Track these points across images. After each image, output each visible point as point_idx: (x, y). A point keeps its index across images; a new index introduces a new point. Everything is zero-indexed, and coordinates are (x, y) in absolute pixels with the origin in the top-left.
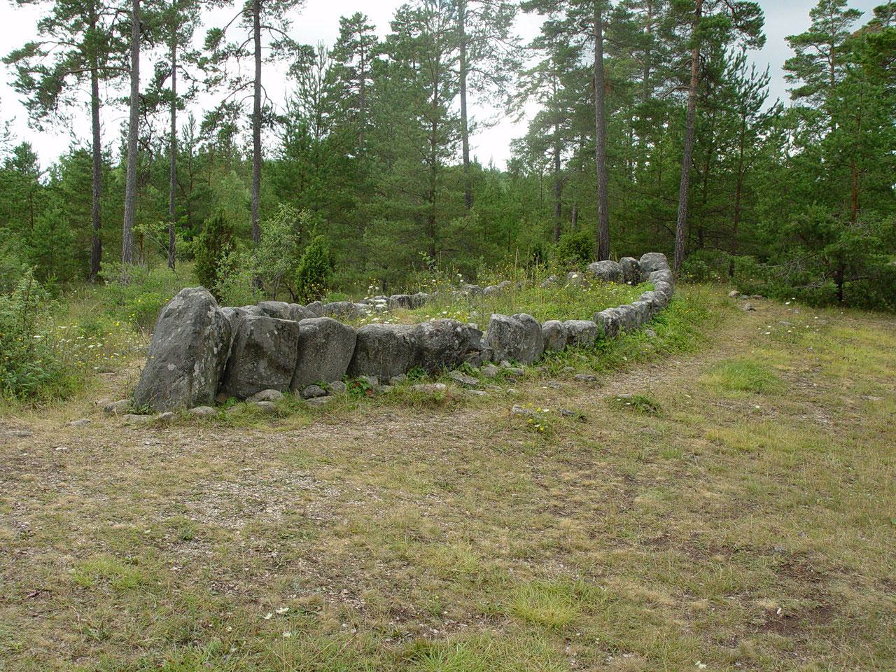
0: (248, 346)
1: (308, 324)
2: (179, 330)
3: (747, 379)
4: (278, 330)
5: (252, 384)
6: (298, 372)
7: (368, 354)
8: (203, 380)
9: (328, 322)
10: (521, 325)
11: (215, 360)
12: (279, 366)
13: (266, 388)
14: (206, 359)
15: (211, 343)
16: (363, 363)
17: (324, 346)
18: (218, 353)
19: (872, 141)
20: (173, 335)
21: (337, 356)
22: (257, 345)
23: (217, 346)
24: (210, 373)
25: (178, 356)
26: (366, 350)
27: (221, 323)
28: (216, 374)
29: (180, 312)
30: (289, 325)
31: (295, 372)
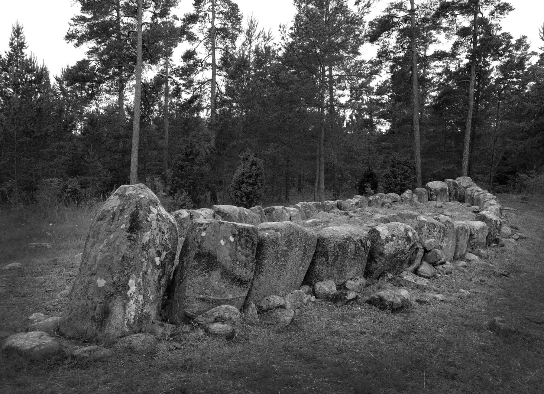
0: (199, 256)
1: (268, 229)
2: (112, 236)
3: (452, 231)
4: (234, 236)
5: (203, 300)
6: (256, 284)
7: (327, 259)
8: (141, 297)
9: (291, 227)
10: (443, 225)
11: (157, 273)
12: (235, 278)
13: (218, 303)
14: (146, 273)
15: (152, 251)
16: (321, 268)
17: (285, 254)
18: (161, 262)
19: (193, 159)
20: (105, 242)
21: (297, 263)
22: (209, 255)
23: (159, 254)
24: (151, 288)
25: (110, 269)
26: (325, 255)
27: (164, 228)
28: (158, 289)
29: (114, 215)
30: (247, 230)
31: (252, 283)
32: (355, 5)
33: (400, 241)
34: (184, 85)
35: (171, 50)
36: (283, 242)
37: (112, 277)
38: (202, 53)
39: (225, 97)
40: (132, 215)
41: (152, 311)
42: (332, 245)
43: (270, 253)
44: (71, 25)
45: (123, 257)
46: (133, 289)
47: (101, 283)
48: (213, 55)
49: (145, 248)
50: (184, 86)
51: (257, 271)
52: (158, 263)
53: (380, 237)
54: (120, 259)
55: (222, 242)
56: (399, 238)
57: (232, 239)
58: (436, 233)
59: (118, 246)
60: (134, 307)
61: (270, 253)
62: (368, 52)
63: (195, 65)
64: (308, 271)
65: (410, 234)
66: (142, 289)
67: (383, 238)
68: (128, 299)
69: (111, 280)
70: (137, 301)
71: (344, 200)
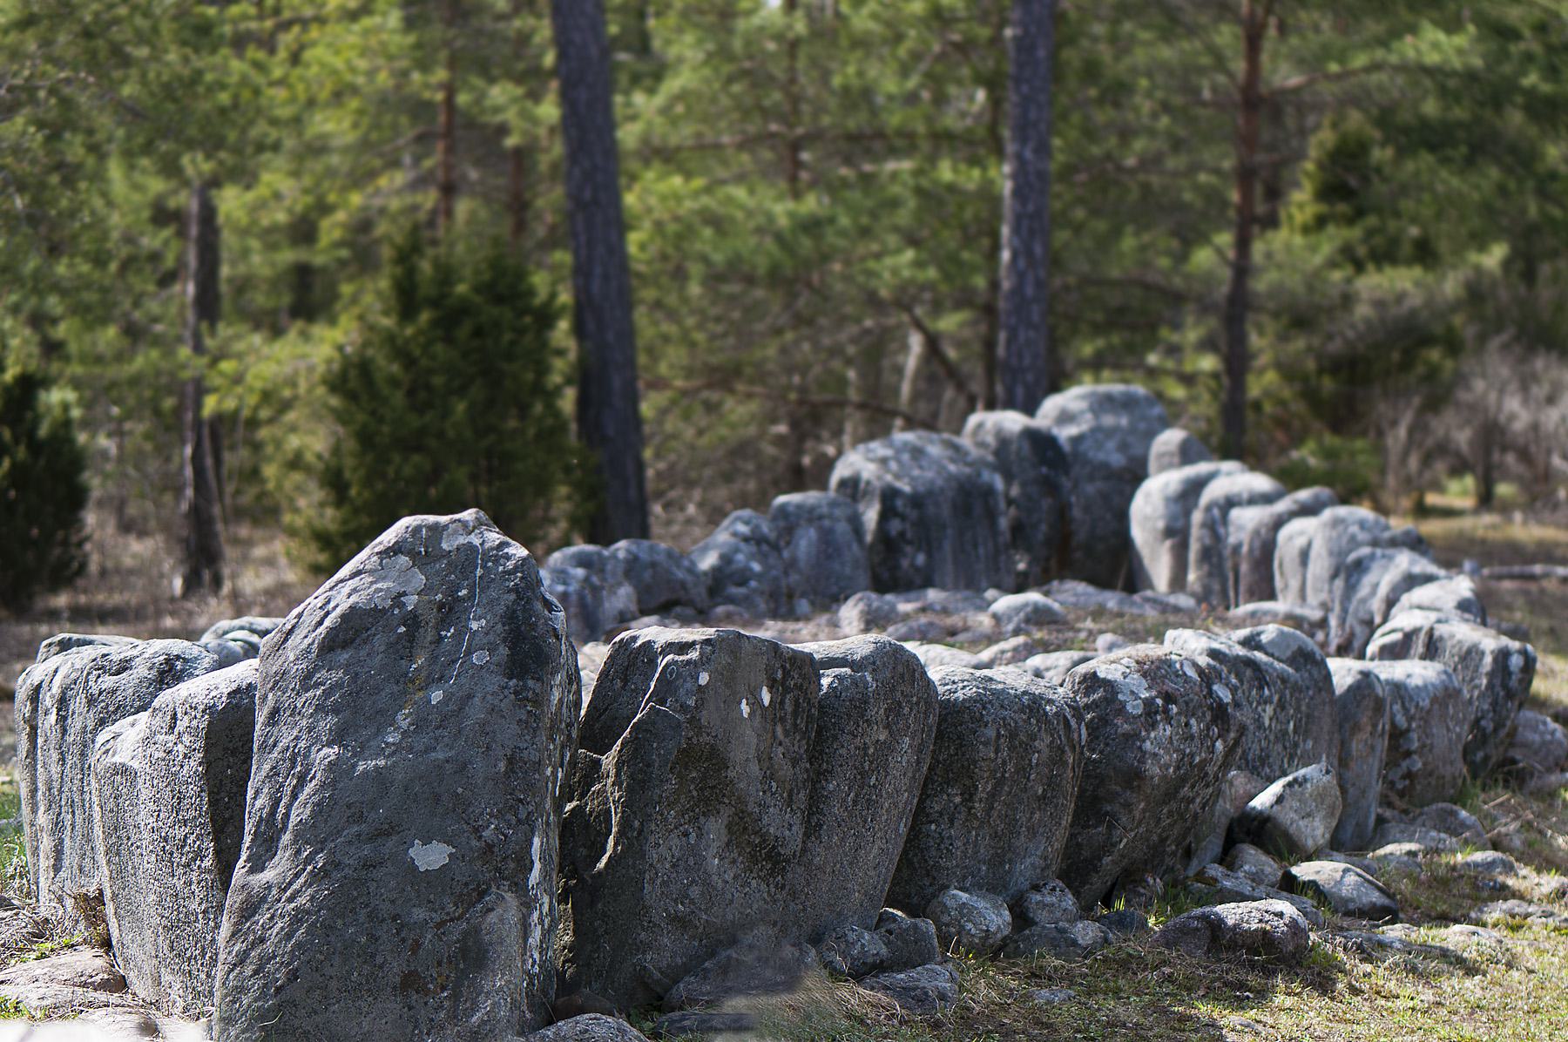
7: (969, 795)
33: (1193, 721)
36: (877, 711)
37: (477, 830)
39: (916, 342)
40: (510, 617)
42: (991, 732)
43: (843, 751)
44: (1439, 621)
45: (511, 761)
47: (431, 856)
51: (812, 829)
53: (1123, 704)
54: (502, 766)
56: (1189, 711)
58: (1269, 709)
59: (483, 724)
61: (843, 751)
64: (905, 852)
65: (1224, 694)
67: (1134, 708)
69: (474, 843)
71: (1546, 651)
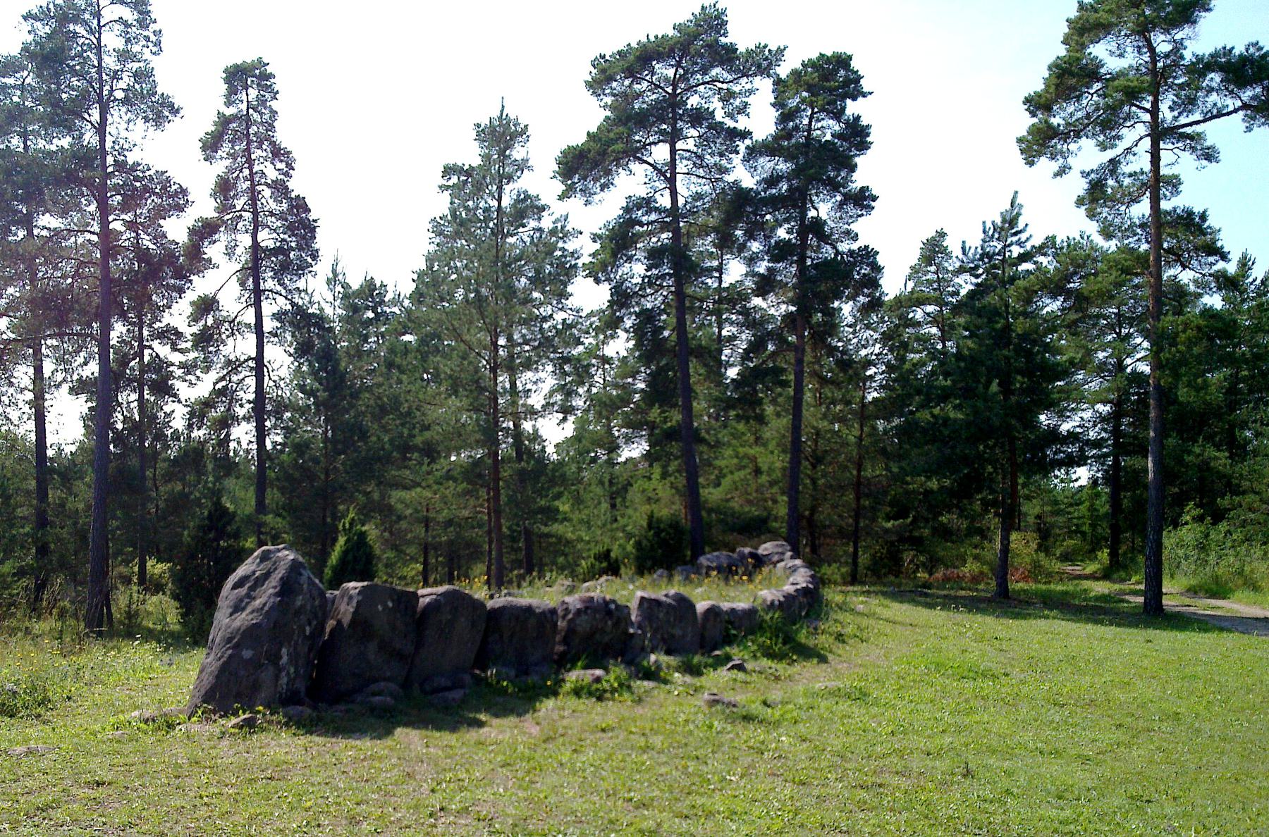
8: (292, 670)
13: (375, 680)
32: (1204, 212)
34: (182, 366)
35: (417, 296)
38: (232, 301)
41: (301, 685)
46: (285, 659)
48: (257, 305)
49: (298, 612)
50: (179, 367)
51: (419, 644)
52: (308, 633)
55: (380, 607)
57: (390, 604)
60: (285, 680)
62: (589, 296)
63: (218, 323)
66: (293, 659)
68: (280, 671)
70: (288, 674)
